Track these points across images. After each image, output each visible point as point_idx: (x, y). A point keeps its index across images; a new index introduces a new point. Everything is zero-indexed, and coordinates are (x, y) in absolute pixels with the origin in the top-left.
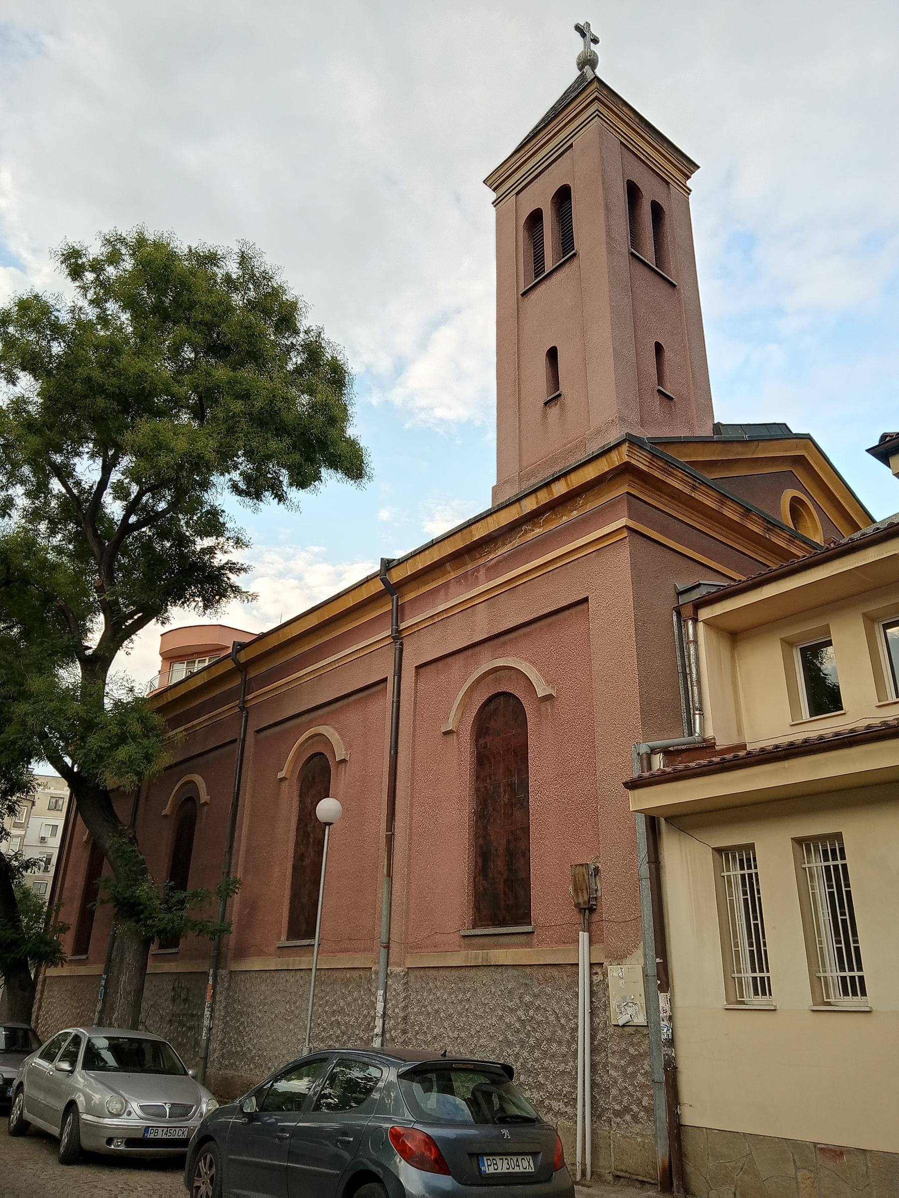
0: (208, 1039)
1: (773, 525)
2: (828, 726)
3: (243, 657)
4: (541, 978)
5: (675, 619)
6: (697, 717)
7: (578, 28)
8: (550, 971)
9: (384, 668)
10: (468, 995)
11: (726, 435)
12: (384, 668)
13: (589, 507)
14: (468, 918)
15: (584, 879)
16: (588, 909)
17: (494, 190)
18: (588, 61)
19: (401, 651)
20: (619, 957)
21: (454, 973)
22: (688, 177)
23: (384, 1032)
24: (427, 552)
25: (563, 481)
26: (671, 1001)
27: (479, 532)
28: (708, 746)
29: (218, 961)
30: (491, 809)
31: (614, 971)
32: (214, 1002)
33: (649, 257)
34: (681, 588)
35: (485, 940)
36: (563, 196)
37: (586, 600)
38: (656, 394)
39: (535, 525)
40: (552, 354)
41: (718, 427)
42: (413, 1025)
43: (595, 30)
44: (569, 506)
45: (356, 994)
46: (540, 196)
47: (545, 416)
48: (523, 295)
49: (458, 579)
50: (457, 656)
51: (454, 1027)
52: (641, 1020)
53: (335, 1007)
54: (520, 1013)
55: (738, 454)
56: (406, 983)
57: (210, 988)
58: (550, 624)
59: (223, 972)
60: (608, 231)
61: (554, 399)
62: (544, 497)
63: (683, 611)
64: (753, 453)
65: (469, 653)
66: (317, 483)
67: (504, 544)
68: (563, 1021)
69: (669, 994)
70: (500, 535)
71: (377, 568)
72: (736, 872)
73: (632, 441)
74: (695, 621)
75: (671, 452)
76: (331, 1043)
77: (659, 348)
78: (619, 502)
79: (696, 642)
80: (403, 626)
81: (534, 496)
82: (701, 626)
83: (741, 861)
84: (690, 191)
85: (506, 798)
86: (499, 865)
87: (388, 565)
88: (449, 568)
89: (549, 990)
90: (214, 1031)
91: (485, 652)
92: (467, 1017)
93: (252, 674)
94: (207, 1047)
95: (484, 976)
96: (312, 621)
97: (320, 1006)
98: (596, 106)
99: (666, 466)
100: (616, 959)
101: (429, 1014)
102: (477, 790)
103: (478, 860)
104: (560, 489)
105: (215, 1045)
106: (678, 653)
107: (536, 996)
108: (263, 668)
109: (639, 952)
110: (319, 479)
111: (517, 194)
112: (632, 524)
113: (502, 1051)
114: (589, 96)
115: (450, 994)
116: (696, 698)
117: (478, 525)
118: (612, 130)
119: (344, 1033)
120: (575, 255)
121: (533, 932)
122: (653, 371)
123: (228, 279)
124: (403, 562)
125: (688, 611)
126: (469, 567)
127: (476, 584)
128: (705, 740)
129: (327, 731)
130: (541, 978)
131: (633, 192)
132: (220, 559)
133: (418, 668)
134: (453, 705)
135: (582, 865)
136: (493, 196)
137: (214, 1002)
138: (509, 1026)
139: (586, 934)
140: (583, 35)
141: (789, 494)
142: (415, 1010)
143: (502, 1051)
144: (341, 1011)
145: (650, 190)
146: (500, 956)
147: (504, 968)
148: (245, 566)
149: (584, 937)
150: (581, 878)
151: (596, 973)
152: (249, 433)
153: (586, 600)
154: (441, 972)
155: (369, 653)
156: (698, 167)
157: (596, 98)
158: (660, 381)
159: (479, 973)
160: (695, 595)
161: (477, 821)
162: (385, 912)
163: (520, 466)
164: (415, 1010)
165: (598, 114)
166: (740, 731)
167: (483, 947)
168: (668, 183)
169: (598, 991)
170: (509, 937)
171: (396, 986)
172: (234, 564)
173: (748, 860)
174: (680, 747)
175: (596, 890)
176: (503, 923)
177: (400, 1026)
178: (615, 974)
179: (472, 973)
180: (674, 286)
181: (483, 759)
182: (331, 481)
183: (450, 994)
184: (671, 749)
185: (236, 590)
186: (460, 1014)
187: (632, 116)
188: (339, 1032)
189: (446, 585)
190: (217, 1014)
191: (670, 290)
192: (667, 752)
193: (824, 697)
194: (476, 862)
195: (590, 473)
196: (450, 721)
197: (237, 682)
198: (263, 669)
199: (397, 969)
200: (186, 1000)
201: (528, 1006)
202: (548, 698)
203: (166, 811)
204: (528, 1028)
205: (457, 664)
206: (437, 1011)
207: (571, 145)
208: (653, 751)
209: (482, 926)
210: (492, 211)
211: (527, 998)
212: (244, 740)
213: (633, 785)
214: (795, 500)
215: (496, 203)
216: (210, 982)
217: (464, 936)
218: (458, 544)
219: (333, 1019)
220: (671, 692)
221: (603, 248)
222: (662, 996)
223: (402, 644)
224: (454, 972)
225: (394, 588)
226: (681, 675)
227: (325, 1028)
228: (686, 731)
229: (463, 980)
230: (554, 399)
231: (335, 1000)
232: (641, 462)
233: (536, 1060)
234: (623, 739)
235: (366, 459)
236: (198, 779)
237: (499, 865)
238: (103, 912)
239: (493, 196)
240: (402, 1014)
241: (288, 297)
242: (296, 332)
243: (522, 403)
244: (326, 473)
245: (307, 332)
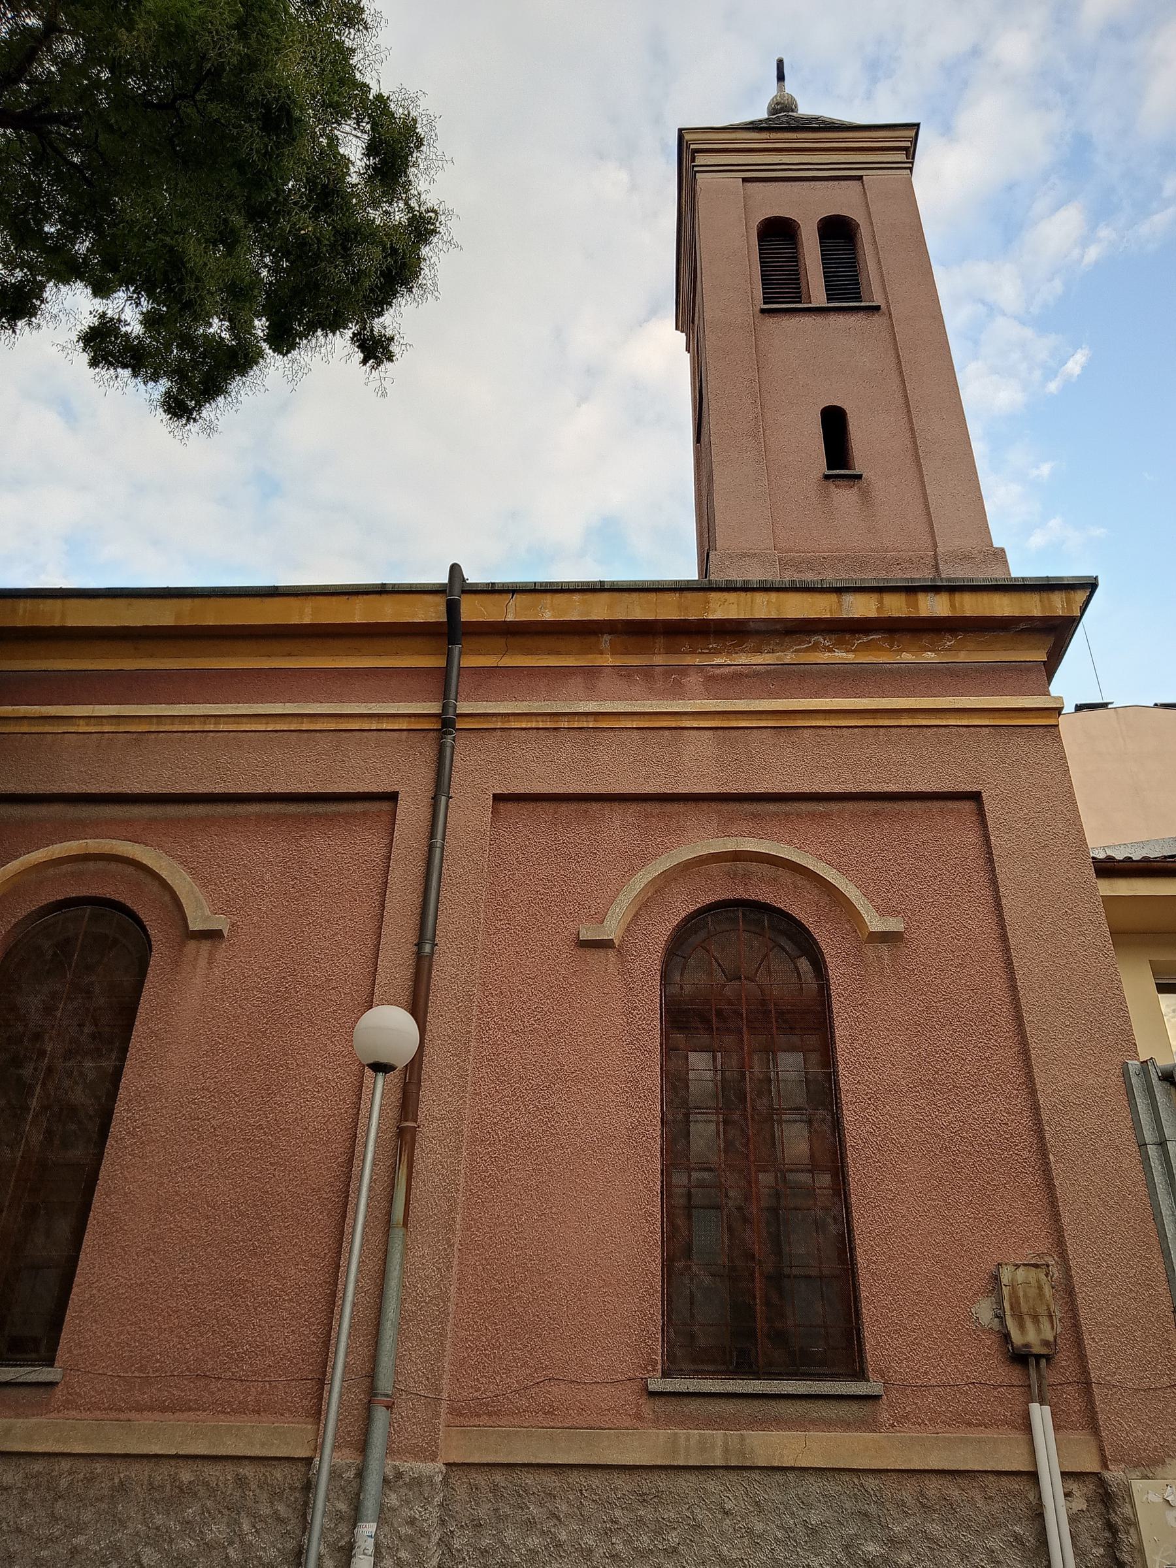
10: (673, 1538)
13: (962, 657)
24: (576, 597)
35: (728, 1407)
39: (840, 644)
44: (925, 640)
58: (876, 814)
62: (896, 606)
65: (656, 808)
67: (759, 651)
70: (758, 633)
89: (935, 1529)
95: (732, 1495)
104: (935, 606)
127: (678, 691)
147: (791, 1476)
150: (1033, 1292)
154: (574, 1478)
167: (711, 1423)
170: (834, 1404)
178: (1155, 1498)
179: (685, 1483)
189: (591, 673)
209: (696, 1372)
224: (619, 1480)
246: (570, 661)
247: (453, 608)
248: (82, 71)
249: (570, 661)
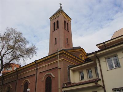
1: (79, 58)
2: (83, 81)
9: (35, 73)
34: (69, 65)
36: (58, 22)
40: (56, 38)
46: (55, 21)
77: (67, 39)
84: (71, 19)
87: (36, 61)
108: (20, 71)
114: (60, 11)
129: (28, 80)
131: (65, 22)
133: (39, 73)
139: (53, 77)
141: (80, 54)
145: (67, 21)
155: (33, 71)
158: (67, 42)
160: (70, 67)
181: (47, 84)
193: (82, 78)
202: (54, 78)
205: (44, 73)
214: (81, 55)
218: (44, 59)
236: (11, 85)
238: (101, 79)
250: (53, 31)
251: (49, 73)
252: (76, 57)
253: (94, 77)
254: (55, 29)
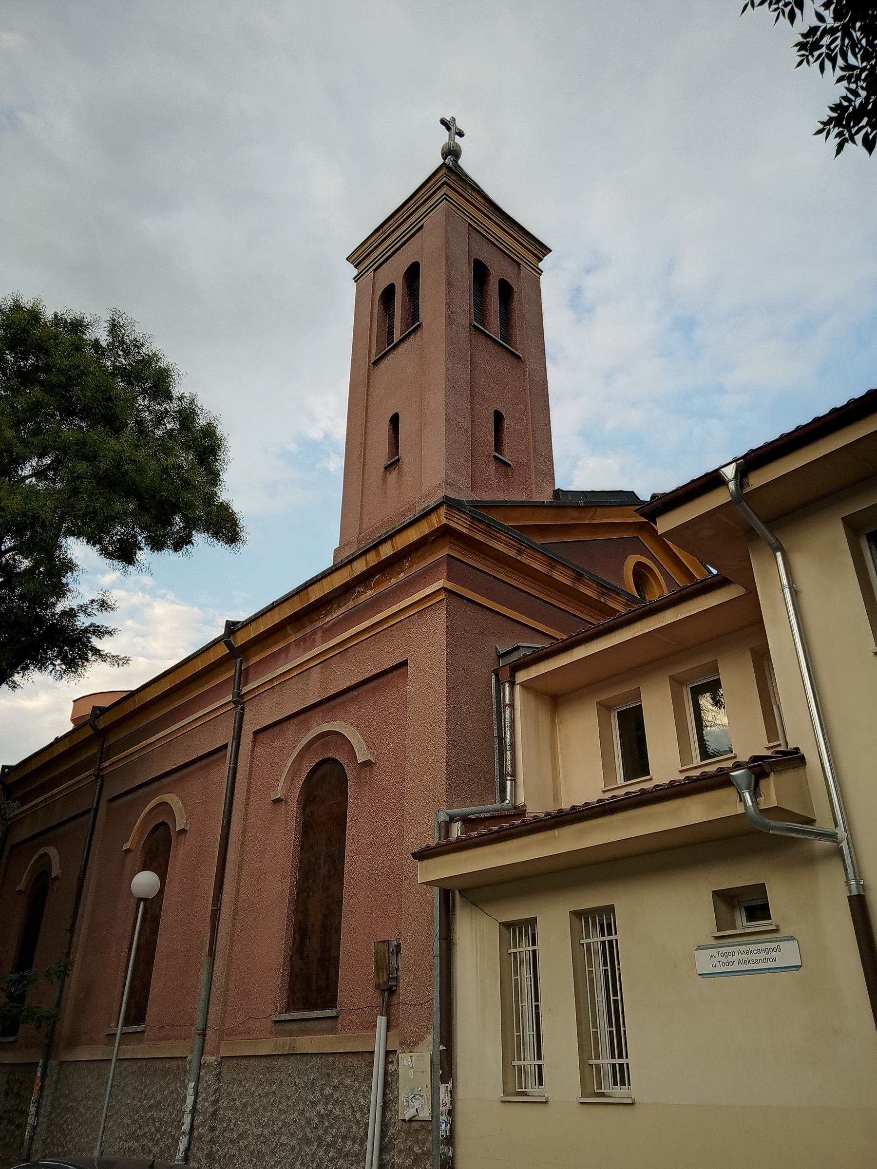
0: (32, 1139)
2: (637, 786)
3: (102, 724)
4: (341, 1067)
5: (493, 681)
6: (509, 783)
7: (443, 122)
8: (350, 1060)
9: (225, 736)
10: (274, 1087)
11: (563, 501)
12: (225, 736)
14: (281, 1003)
15: (385, 957)
16: (389, 990)
17: (356, 267)
18: (452, 153)
19: (242, 716)
20: (411, 1044)
21: (263, 1062)
22: (541, 260)
23: (192, 1128)
24: (268, 614)
25: (389, 543)
26: (452, 1093)
27: (315, 594)
28: (520, 812)
29: (49, 1049)
30: (311, 881)
31: (405, 1060)
32: (41, 1096)
33: (494, 328)
34: (501, 650)
35: (294, 1026)
36: (413, 273)
37: (405, 663)
38: (491, 459)
39: (368, 587)
40: (395, 420)
41: (558, 493)
42: (222, 1120)
43: (460, 125)
45: (172, 1087)
46: (393, 273)
47: (384, 480)
48: (373, 364)
49: (297, 642)
50: (292, 721)
51: (258, 1124)
52: (425, 1114)
53: (152, 1102)
54: (320, 1107)
55: (572, 519)
56: (219, 1074)
57: (38, 1080)
59: (53, 1063)
60: (449, 305)
61: (393, 464)
62: (372, 559)
63: (500, 673)
64: (592, 518)
65: (302, 717)
66: (188, 547)
68: (358, 1115)
69: (450, 1086)
70: (336, 597)
71: (220, 631)
72: (596, 940)
73: (449, 503)
74: (512, 684)
75: (495, 516)
76: (145, 1142)
77: (498, 417)
78: (440, 564)
79: (512, 705)
80: (245, 690)
81: (363, 558)
82: (518, 688)
83: (602, 926)
84: (541, 250)
85: (324, 870)
86: (314, 942)
88: (290, 631)
90: (38, 1130)
91: (317, 714)
92: (272, 1112)
93: (112, 740)
94: (30, 1148)
96: (165, 686)
97: (139, 1100)
98: (445, 190)
99: (488, 529)
100: (409, 1046)
101: (237, 1108)
102: (301, 861)
103: (297, 936)
104: (387, 551)
105: (37, 1145)
106: (495, 716)
107: (336, 1088)
108: (123, 733)
109: (429, 1038)
110: (190, 542)
111: (375, 270)
112: (449, 585)
113: (300, 1150)
115: (258, 1085)
116: (509, 763)
117: (315, 587)
118: (454, 208)
119: (158, 1130)
120: (419, 326)
121: (337, 1017)
122: (491, 438)
123: (96, 344)
124: (246, 625)
125: (505, 674)
126: (308, 630)
128: (515, 808)
129: (173, 799)
130: (341, 1067)
131: (480, 272)
132: (83, 621)
133: (257, 733)
134: (280, 774)
135: (384, 941)
136: (355, 272)
137: (41, 1096)
138: (309, 1121)
139: (384, 1018)
140: (449, 129)
142: (225, 1104)
143: (300, 1150)
144: (157, 1106)
145: (498, 269)
146: (307, 1043)
148: (110, 629)
149: (381, 1021)
150: (382, 955)
151: (392, 1062)
152: (93, 493)
153: (405, 663)
154: (252, 1060)
156: (551, 251)
157: (445, 183)
159: (286, 1063)
160: (514, 657)
161: (298, 895)
162: (203, 996)
163: (361, 528)
164: (225, 1104)
165: (446, 198)
166: (556, 797)
167: (291, 1034)
168: (519, 264)
169: (389, 1082)
170: (316, 1022)
171: (209, 1078)
172: (98, 626)
173: (609, 925)
174: (482, 815)
175: (397, 969)
176: (314, 1007)
177: (208, 1123)
179: (281, 1061)
180: (519, 358)
181: (308, 828)
182: (202, 542)
183: (258, 1085)
184: (472, 817)
185: (96, 652)
186: (265, 1108)
187: (482, 201)
188: (153, 1130)
189: (286, 648)
190: (42, 1111)
191: (515, 362)
192: (466, 821)
193: (637, 761)
194: (294, 939)
195: (413, 535)
196: (279, 788)
197: (94, 750)
198: (122, 735)
199: (209, 1059)
200: (18, 1095)
201: (328, 1099)
202: (367, 764)
203: (21, 887)
204: (326, 1124)
205: (291, 729)
206: (244, 1106)
207: (422, 227)
208: (452, 819)
210: (353, 286)
211: (328, 1091)
212: (97, 810)
213: (422, 855)
214: (639, 564)
215: (356, 279)
216: (39, 1074)
217: (276, 1022)
218: (295, 606)
219: (149, 1114)
220: (482, 756)
221: (443, 320)
222: (443, 1087)
223: (243, 709)
225: (239, 651)
226: (496, 741)
227: (141, 1126)
228: (498, 797)
229: (270, 1070)
230: (393, 464)
231: (153, 1093)
232: (461, 525)
233: (331, 1160)
234: (427, 808)
235: (241, 523)
236: (52, 851)
237: (314, 942)
239: (355, 272)
240: (211, 1109)
241: (162, 364)
242: (170, 398)
243: (367, 467)
244: (199, 538)
245: (181, 398)
246: (276, 648)
247: (229, 644)
248: (11, 526)
249: (276, 648)
250: (376, 363)
251: (327, 727)
252: (579, 576)
253: (751, 743)
254: (390, 341)
